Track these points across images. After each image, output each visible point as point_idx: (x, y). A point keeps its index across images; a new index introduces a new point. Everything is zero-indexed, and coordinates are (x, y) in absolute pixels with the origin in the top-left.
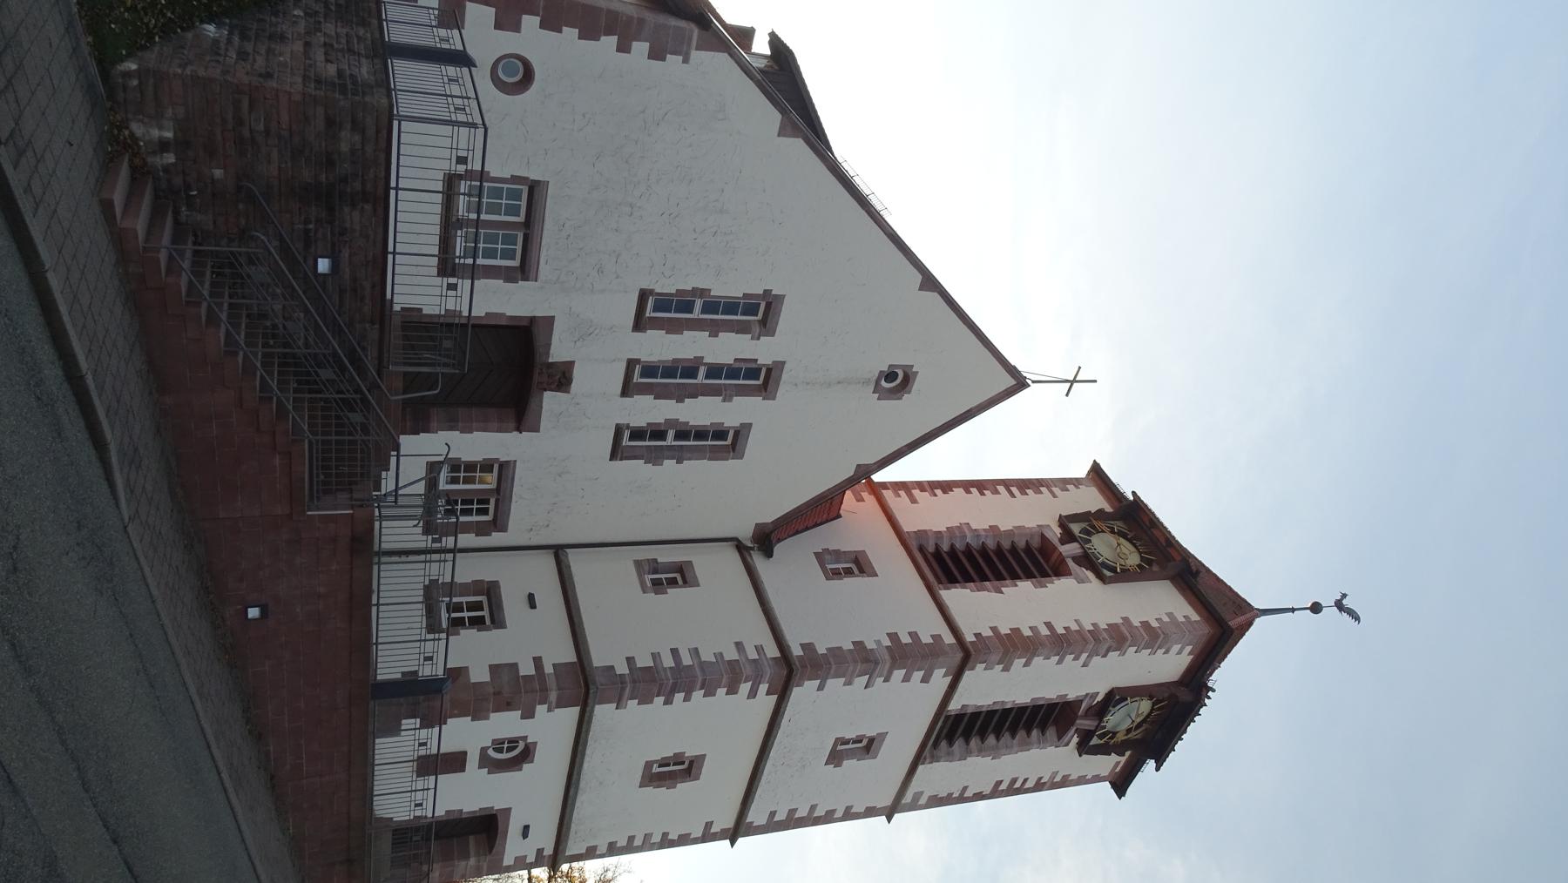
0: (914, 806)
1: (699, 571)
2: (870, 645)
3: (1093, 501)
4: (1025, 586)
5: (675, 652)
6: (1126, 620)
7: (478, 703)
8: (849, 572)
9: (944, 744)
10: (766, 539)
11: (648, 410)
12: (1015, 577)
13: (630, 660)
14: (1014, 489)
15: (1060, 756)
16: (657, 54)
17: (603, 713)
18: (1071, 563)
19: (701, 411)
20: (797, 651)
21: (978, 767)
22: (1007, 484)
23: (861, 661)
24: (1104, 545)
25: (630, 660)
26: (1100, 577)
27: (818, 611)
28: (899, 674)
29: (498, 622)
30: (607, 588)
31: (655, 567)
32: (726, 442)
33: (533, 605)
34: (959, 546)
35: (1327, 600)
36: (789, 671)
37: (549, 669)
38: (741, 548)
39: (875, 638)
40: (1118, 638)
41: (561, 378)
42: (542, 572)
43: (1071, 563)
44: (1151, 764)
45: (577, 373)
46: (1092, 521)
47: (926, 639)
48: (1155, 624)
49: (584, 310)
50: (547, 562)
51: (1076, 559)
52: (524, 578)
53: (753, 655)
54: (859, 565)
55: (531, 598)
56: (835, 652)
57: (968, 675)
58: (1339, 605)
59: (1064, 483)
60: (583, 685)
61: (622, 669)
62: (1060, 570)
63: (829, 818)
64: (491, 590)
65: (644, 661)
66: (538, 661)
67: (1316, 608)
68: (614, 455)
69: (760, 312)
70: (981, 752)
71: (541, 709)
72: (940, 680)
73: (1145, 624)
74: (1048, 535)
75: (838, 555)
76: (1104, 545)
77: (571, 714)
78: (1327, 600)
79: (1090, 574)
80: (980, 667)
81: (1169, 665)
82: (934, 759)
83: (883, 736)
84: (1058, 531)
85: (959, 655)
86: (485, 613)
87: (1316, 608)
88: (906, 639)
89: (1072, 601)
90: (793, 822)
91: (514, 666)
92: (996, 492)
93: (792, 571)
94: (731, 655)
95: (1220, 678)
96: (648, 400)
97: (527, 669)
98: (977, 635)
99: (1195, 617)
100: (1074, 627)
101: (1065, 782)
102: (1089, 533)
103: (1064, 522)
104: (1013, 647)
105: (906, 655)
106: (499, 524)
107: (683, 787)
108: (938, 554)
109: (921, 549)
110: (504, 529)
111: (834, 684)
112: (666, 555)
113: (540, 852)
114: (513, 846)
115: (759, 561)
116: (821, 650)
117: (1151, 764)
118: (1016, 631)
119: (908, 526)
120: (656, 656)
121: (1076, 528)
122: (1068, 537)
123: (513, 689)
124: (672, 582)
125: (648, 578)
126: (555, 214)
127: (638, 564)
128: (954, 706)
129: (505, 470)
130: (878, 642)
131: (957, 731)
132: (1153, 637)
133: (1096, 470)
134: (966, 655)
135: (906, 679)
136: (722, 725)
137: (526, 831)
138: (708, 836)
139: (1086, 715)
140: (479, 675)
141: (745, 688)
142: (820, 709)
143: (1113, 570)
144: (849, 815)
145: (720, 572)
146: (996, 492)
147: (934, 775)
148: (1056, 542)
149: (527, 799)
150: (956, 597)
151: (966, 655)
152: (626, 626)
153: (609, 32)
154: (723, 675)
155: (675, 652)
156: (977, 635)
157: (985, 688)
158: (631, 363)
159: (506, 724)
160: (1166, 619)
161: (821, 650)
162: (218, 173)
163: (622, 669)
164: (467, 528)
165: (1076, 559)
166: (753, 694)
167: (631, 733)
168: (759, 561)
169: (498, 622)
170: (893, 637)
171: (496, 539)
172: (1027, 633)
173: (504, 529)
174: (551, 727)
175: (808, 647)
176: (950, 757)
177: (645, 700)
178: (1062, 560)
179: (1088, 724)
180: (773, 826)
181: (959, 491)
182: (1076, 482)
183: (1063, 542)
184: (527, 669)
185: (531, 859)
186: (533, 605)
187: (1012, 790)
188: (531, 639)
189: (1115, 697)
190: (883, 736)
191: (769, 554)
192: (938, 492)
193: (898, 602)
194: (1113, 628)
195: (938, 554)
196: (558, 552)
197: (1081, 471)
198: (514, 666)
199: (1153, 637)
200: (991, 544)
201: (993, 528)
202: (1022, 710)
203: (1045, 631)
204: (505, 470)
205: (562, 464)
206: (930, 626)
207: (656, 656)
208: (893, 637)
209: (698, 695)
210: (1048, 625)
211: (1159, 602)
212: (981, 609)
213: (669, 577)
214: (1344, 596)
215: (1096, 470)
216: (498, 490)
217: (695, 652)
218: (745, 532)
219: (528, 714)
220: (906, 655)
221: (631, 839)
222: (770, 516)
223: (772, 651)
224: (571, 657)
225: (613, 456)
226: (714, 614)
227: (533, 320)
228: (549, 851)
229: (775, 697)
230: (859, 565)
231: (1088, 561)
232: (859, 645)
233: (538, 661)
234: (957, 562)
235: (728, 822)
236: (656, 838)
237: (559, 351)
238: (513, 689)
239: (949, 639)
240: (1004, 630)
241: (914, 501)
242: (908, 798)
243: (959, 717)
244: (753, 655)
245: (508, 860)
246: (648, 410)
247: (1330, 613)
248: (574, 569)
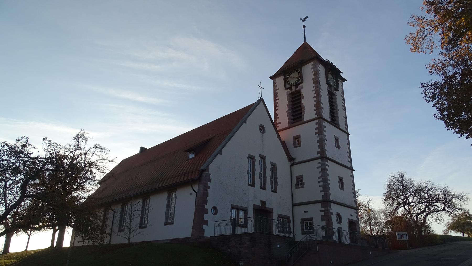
0: (347, 129)
1: (299, 174)
2: (318, 139)
3: (280, 80)
4: (303, 101)
5: (319, 182)
6: (312, 79)
7: (329, 223)
8: (298, 141)
9: (336, 122)
10: (291, 159)
11: (268, 185)
12: (301, 102)
13: (321, 191)
14: (277, 98)
15: (338, 94)
16: (210, 181)
17: (332, 198)
18: (297, 89)
19: (268, 173)
20: (319, 155)
21: (340, 114)
22: (275, 100)
23: (321, 142)
24: (293, 81)
25: (321, 191)
26: (301, 83)
27: (309, 148)
28: (324, 133)
29: (311, 219)
30: (302, 195)
31: (297, 184)
32: (274, 166)
33: (307, 212)
34: (291, 114)
35: (302, 24)
36: (323, 157)
37: (323, 209)
38: (292, 165)
39: (316, 138)
40: (316, 82)
41: (263, 203)
42: (299, 210)
43: (297, 89)
44: (341, 74)
45: (262, 200)
46: (286, 82)
47: (317, 126)
48: (314, 73)
49: (253, 197)
50: (296, 208)
51: (296, 88)
52: (300, 213)
53: (320, 165)
54: (297, 139)
55: (305, 212)
56: (319, 147)
57: (324, 117)
58: (304, 21)
59: (275, 86)
60: (326, 202)
61: (323, 193)
62: (299, 92)
63: (349, 148)
64: (303, 220)
65: (321, 189)
66: (321, 211)
67: (304, 27)
68: (276, 192)
69: (251, 158)
70: (337, 114)
71: (331, 211)
72: (325, 124)
73: (314, 75)
74: (289, 93)
75: (294, 143)
76: (293, 81)
77: (332, 205)
78: (302, 24)
79: (300, 85)
80: (323, 114)
81: (322, 69)
82: (339, 125)
83: (335, 137)
84: (288, 90)
85: (321, 119)
86: (308, 222)
87: (304, 27)
88: (317, 131)
89: (307, 90)
90: (350, 157)
91: (322, 216)
92: (277, 103)
93: (299, 154)
94: (320, 170)
95: (325, 58)
96: (267, 184)
97: (323, 213)
98: (316, 114)
99: (312, 63)
100: (314, 92)
101: (343, 93)
102: (289, 83)
103: (286, 89)
104: (318, 107)
105: (320, 131)
106: (288, 218)
107: (344, 181)
108: (294, 119)
109: (292, 123)
110: (289, 217)
111: (326, 147)
112: (295, 181)
113: (355, 213)
114: (354, 218)
115: (296, 161)
116: (319, 150)
117: (341, 74)
118: (315, 105)
119: (287, 125)
120: (320, 186)
121: (288, 86)
122: (290, 88)
123: (327, 217)
124: (301, 181)
125: (300, 186)
126: (236, 204)
127: (296, 188)
128: (329, 120)
129: (279, 216)
130: (317, 137)
131: (334, 121)
132: (316, 74)
133: (271, 78)
134: (320, 117)
135: (325, 131)
136: (334, 172)
137: (351, 215)
138: (352, 176)
139: (331, 89)
140: (324, 223)
141: (327, 167)
142: (331, 152)
143: (299, 80)
144: (349, 144)
145: (298, 170)
146: (277, 103)
147: (342, 126)
148: (291, 91)
149: (346, 214)
150: (306, 117)
151: (320, 117)
152: (312, 191)
153: (207, 191)
154: (324, 171)
155: (319, 182)
156: (316, 114)
157: (326, 114)
158: (261, 188)
159: (334, 218)
160: (312, 70)
161: (319, 150)
162: (269, 263)
163: (323, 193)
164: (289, 225)
165: (296, 88)
166: (328, 166)
167: (335, 193)
168: (296, 161)
169: (311, 219)
170: (316, 133)
171: (291, 219)
172: (315, 103)
173: (289, 217)
174: (334, 209)
175: (318, 153)
176: (338, 121)
177: (329, 189)
178: (296, 91)
179: (333, 88)
180: (351, 161)
181: (277, 112)
182: (275, 83)
183: (291, 90)
184: (323, 213)
185: (356, 215)
186: (307, 212)
187: (344, 106)
188: (315, 213)
189: (328, 83)
190: (335, 137)
191: (294, 159)
192: (277, 117)
193: (307, 131)
194: (314, 83)
195: (294, 119)
196: (294, 205)
197: (272, 81)
198: (322, 216)
199: (316, 74)
200: (291, 106)
201: (287, 105)
202: (330, 104)
203: (315, 99)
204: (279, 216)
205: (279, 203)
206: (313, 125)
207: (320, 186)
208: (316, 133)
209: (328, 178)
210: (314, 98)
211: (308, 70)
212: (309, 112)
213: (300, 182)
214: (301, 19)
215: (271, 78)
216: (282, 218)
217: (319, 178)
218: (289, 164)
219: (332, 214)
220: (320, 131)
221: (353, 193)
222: (286, 158)
223: (319, 161)
224: (320, 204)
225: (276, 192)
226: (310, 172)
227: (254, 209)
228: (355, 211)
229: (329, 161)
230: (297, 139)
231: (297, 85)
232: (318, 141)
233: (321, 211)
234: (296, 115)
235: (350, 171)
236: (353, 187)
237: (259, 204)
238: (327, 217)
239: (317, 121)
240: (315, 108)
241: (280, 123)
242: (346, 130)
243: (331, 119)
244: (320, 165)
245: (356, 219)
246: (268, 185)
247: (306, 23)
248: (298, 202)
